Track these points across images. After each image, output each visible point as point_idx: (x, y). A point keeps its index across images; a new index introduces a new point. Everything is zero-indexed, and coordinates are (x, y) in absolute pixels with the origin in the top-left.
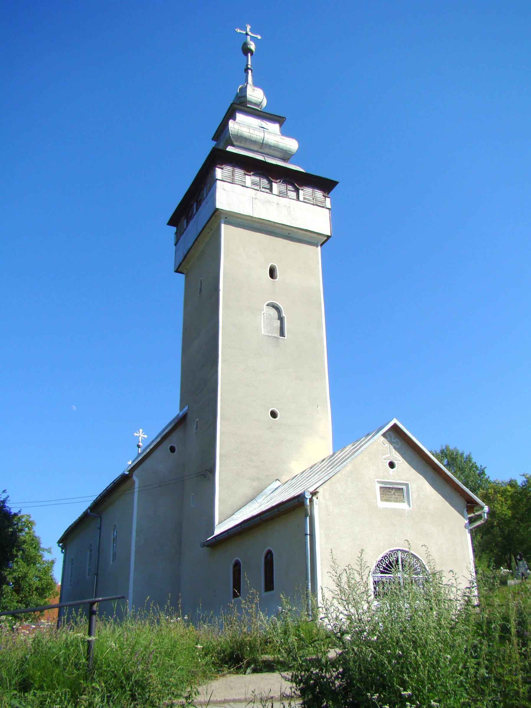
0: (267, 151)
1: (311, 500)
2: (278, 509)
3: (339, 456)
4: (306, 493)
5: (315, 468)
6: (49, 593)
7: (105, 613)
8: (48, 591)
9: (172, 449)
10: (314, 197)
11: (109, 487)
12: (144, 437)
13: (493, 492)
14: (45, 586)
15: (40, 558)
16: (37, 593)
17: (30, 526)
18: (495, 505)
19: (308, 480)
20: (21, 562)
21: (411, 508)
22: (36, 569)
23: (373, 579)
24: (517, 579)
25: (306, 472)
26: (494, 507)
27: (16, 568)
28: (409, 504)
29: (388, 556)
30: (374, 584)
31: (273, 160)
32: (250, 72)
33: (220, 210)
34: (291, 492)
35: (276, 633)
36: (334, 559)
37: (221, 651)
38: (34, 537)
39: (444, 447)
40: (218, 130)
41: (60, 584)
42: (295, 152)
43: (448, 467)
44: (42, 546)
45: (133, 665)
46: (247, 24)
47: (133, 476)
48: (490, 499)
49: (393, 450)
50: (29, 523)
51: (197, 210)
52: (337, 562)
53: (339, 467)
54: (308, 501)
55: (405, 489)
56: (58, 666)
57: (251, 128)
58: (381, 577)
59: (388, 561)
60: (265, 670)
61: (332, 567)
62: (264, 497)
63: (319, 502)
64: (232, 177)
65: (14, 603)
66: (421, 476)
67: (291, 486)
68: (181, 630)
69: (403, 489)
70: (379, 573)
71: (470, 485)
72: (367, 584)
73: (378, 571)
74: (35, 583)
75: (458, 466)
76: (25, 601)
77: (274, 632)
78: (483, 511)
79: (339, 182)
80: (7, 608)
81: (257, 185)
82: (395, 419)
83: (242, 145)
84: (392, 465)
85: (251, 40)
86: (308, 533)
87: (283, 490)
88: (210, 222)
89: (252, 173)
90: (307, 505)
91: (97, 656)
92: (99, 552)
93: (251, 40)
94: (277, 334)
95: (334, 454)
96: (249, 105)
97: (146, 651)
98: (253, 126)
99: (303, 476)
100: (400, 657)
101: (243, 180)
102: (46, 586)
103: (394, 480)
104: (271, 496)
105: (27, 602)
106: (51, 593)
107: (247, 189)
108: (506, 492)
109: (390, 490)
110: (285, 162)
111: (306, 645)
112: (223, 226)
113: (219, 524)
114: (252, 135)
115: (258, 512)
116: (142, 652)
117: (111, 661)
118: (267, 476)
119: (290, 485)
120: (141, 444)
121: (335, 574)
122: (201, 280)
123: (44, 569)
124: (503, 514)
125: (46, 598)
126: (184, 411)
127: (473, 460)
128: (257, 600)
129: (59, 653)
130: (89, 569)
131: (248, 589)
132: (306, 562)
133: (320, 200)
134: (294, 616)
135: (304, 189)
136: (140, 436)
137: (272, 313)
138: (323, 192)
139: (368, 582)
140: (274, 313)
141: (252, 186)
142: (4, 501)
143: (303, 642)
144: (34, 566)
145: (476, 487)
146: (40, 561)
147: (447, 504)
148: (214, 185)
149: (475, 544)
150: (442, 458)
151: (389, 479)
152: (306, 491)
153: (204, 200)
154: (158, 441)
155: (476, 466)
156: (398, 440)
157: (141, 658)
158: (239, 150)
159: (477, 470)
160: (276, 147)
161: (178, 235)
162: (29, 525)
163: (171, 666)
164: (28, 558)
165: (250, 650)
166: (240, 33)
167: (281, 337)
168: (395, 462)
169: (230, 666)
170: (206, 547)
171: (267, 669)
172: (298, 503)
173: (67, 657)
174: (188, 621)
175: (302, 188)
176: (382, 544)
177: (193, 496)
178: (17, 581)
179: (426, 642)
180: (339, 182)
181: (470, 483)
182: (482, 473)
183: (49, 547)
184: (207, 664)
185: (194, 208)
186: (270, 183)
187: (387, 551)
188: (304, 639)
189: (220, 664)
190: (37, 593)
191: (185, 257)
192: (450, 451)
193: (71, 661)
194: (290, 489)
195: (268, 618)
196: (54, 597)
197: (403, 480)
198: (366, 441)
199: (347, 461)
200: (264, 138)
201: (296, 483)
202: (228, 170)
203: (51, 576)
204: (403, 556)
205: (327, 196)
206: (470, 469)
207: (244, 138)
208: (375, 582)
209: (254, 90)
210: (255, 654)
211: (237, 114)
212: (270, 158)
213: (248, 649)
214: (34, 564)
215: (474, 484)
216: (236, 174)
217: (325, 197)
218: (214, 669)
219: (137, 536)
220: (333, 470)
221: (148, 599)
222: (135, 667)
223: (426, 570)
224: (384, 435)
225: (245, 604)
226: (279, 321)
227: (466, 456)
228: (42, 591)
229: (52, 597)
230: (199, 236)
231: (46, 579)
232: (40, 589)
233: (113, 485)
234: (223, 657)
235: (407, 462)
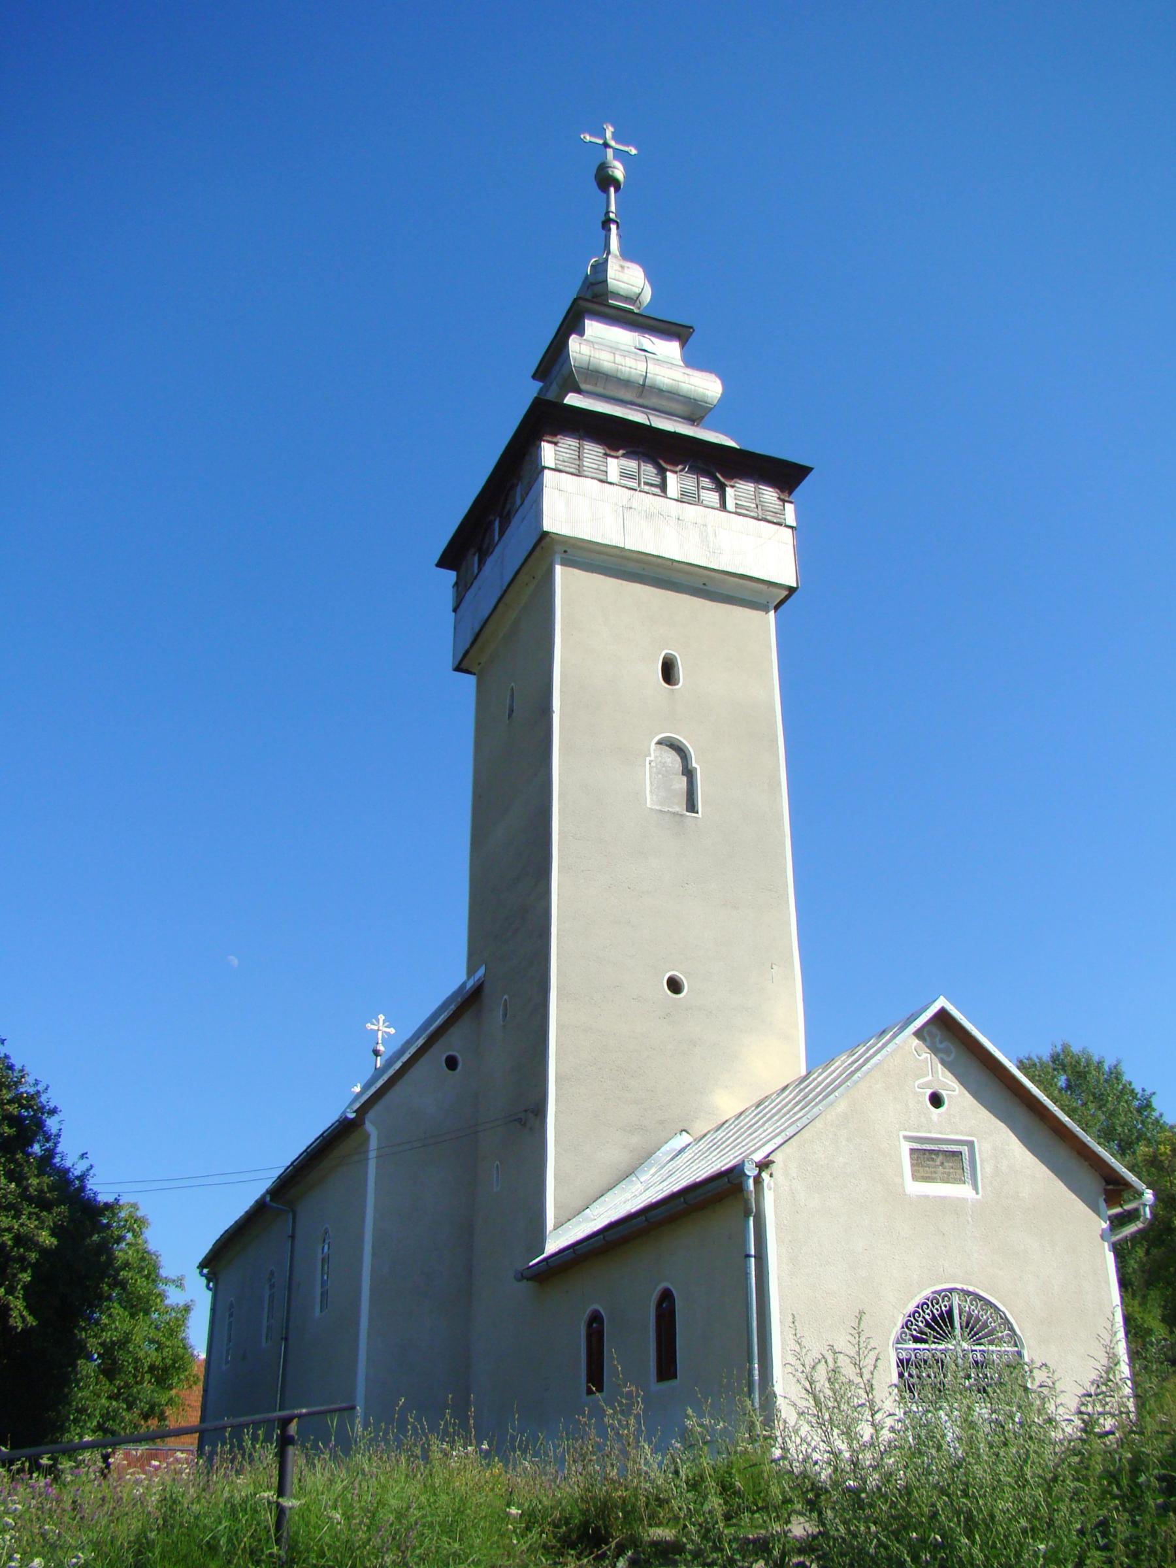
0: (654, 401)
1: (758, 1180)
2: (684, 1199)
3: (820, 1079)
4: (746, 1164)
5: (766, 1107)
6: (178, 1378)
7: (312, 1437)
8: (177, 1374)
9: (452, 1063)
10: (758, 502)
11: (312, 1147)
12: (384, 1022)
13: (1171, 1150)
14: (169, 1362)
15: (158, 1300)
16: (151, 1378)
17: (138, 1229)
19: (751, 1134)
20: (117, 1309)
21: (979, 1197)
22: (151, 1324)
23: (898, 1354)
25: (747, 1114)
26: (1171, 1186)
27: (106, 1321)
28: (976, 1188)
29: (930, 1304)
30: (898, 1366)
31: (665, 421)
32: (613, 227)
33: (550, 535)
34: (714, 1159)
35: (679, 1491)
36: (798, 1336)
37: (560, 1520)
38: (146, 1252)
41: (203, 1356)
42: (715, 402)
43: (1069, 1093)
44: (164, 1272)
45: (373, 1554)
46: (606, 123)
47: (364, 1123)
48: (1163, 1166)
49: (940, 1066)
50: (136, 1221)
51: (502, 534)
52: (804, 1342)
53: (820, 1107)
54: (751, 1181)
55: (967, 1153)
56: (216, 1553)
57: (617, 353)
58: (915, 1349)
59: (929, 1314)
60: (657, 1563)
61: (793, 1352)
62: (653, 1170)
63: (775, 1184)
65: (101, 1399)
66: (1002, 1124)
67: (715, 1145)
68: (473, 1474)
69: (961, 1153)
70: (911, 1342)
71: (1119, 1134)
72: (872, 1385)
73: (908, 1337)
74: (147, 1355)
75: (1090, 1090)
76: (125, 1396)
77: (674, 1489)
78: (1141, 1202)
79: (812, 469)
80: (87, 1410)
81: (631, 477)
82: (942, 997)
83: (600, 390)
84: (936, 1100)
85: (615, 158)
86: (753, 1252)
87: (696, 1154)
89: (621, 452)
90: (748, 1191)
91: (297, 1533)
93: (615, 158)
94: (680, 807)
95: (809, 1074)
96: (611, 300)
97: (400, 1522)
98: (622, 347)
99: (742, 1124)
100: (937, 1546)
102: (171, 1362)
103: (941, 1133)
104: (671, 1168)
105: (131, 1399)
106: (182, 1377)
109: (933, 1156)
110: (693, 425)
111: (747, 1507)
112: (558, 569)
113: (555, 1230)
114: (620, 367)
115: (642, 1205)
116: (391, 1525)
117: (327, 1545)
118: (661, 1122)
119: (711, 1144)
120: (381, 1048)
121: (801, 1368)
122: (512, 689)
123: (168, 1323)
125: (171, 1389)
126: (476, 979)
127: (1126, 1078)
128: (639, 1408)
129: (216, 1528)
130: (268, 1327)
132: (748, 1303)
133: (772, 507)
134: (720, 1441)
135: (737, 485)
136: (378, 1030)
138: (777, 490)
139: (874, 1382)
140: (672, 759)
141: (622, 481)
142: (81, 1176)
143: (741, 1501)
144: (146, 1317)
145: (1134, 1137)
146: (158, 1307)
147: (1060, 1186)
148: (539, 479)
149: (1131, 1269)
150: (1056, 1073)
151: (930, 1132)
152: (746, 1160)
153: (517, 510)
154: (419, 1046)
155: (1132, 1091)
156: (949, 1044)
157: (390, 1539)
158: (591, 401)
159: (1134, 1098)
160: (674, 394)
161: (460, 588)
162: (135, 1226)
163: (455, 1554)
164: (132, 1298)
165: (625, 1517)
166: (590, 142)
167: (688, 814)
168: (944, 1093)
169: (581, 1553)
171: (661, 1560)
172: (729, 1185)
173: (234, 1537)
174: (487, 1455)
175: (732, 484)
177: (497, 1166)
178: (108, 1350)
179: (992, 1516)
180: (812, 469)
181: (1119, 1129)
182: (1147, 1106)
183: (179, 1275)
184: (531, 1550)
185: (494, 530)
186: (662, 472)
187: (927, 1292)
188: (742, 1494)
189: (559, 1549)
190: (151, 1378)
191: (477, 636)
192: (1072, 1057)
193: (243, 1545)
194: (712, 1152)
195: (660, 1458)
196: (191, 1387)
197: (962, 1133)
198: (879, 1048)
199: (836, 1093)
200: (646, 373)
201: (724, 1139)
202: (567, 446)
203: (184, 1339)
205: (787, 499)
206: (1118, 1097)
207: (604, 374)
208: (901, 1361)
209: (622, 267)
210: (636, 1526)
212: (661, 417)
213: (620, 1514)
214: (147, 1312)
215: (1129, 1130)
216: (585, 455)
217: (784, 501)
218: (547, 1560)
219: (374, 1255)
220: (807, 1113)
221: (401, 1403)
222: (377, 1558)
224: (918, 1034)
225: (612, 1417)
226: (685, 779)
227: (1110, 1069)
228: (163, 1375)
229: (185, 1387)
230: (505, 592)
231: (173, 1347)
232: (158, 1368)
233: (319, 1143)
234: (565, 1533)
235: (970, 1094)
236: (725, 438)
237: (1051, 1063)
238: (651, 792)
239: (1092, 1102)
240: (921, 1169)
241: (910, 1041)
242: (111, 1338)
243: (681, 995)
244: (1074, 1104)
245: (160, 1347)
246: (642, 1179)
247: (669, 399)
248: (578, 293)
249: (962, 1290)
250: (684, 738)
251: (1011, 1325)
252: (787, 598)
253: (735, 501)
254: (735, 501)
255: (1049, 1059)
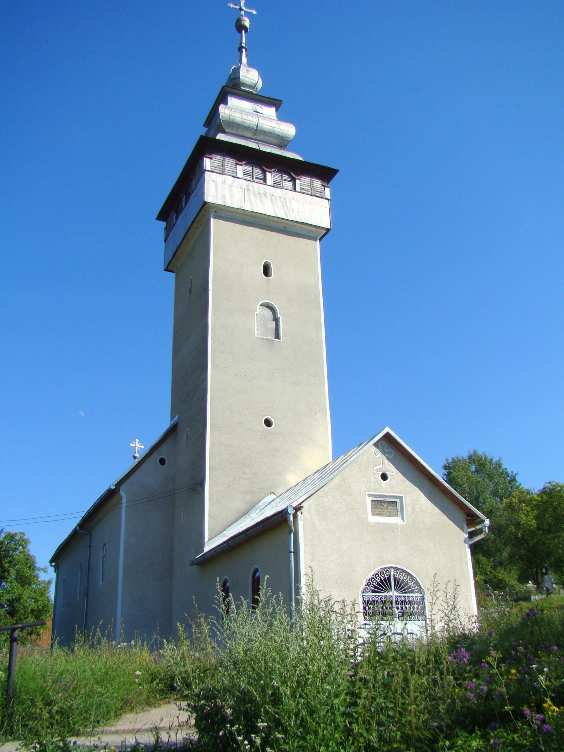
0: (261, 137)
1: (295, 516)
9: (162, 462)
10: (312, 187)
12: (140, 448)
13: (518, 501)
14: (41, 608)
15: (35, 579)
17: (25, 545)
18: (520, 515)
21: (405, 523)
24: (541, 594)
28: (403, 519)
30: (363, 604)
32: (244, 51)
39: (472, 452)
40: (209, 116)
42: (292, 137)
44: (38, 565)
49: (386, 460)
54: (291, 516)
59: (379, 579)
62: (258, 511)
63: (304, 517)
64: (222, 168)
66: (417, 488)
69: (396, 502)
79: (338, 171)
81: (249, 175)
82: (387, 427)
83: (235, 132)
84: (384, 477)
86: (293, 550)
88: (200, 216)
89: (244, 162)
92: (89, 573)
94: (272, 337)
101: (234, 170)
103: (386, 493)
107: (239, 179)
108: (532, 500)
110: (281, 149)
112: (212, 220)
113: (209, 541)
120: (137, 455)
122: (191, 279)
124: (528, 525)
127: (503, 467)
131: (196, 613)
135: (302, 179)
136: (136, 446)
137: (266, 314)
140: (268, 313)
147: (445, 517)
153: (193, 192)
155: (507, 473)
156: (391, 450)
158: (230, 137)
167: (275, 340)
168: (388, 473)
170: (196, 565)
172: (282, 518)
175: (299, 178)
176: (372, 561)
180: (338, 171)
181: (500, 491)
182: (514, 480)
186: (264, 172)
187: (378, 569)
197: (396, 493)
203: (48, 597)
204: (395, 574)
205: (326, 185)
208: (365, 601)
209: (248, 71)
211: (229, 98)
214: (30, 584)
215: (505, 491)
216: (226, 164)
217: (325, 187)
223: (421, 588)
224: (376, 445)
226: (274, 323)
231: (42, 601)
232: (35, 611)
236: (296, 155)
237: (468, 460)
238: (257, 329)
239: (487, 478)
240: (376, 510)
241: (372, 448)
242: (12, 596)
243: (271, 428)
244: (479, 479)
245: (36, 601)
246: (251, 516)
247: (270, 136)
248: (227, 83)
249: (396, 567)
250: (274, 303)
251: (419, 584)
252: (326, 234)
253: (300, 187)
254: (300, 187)
255: (467, 458)
